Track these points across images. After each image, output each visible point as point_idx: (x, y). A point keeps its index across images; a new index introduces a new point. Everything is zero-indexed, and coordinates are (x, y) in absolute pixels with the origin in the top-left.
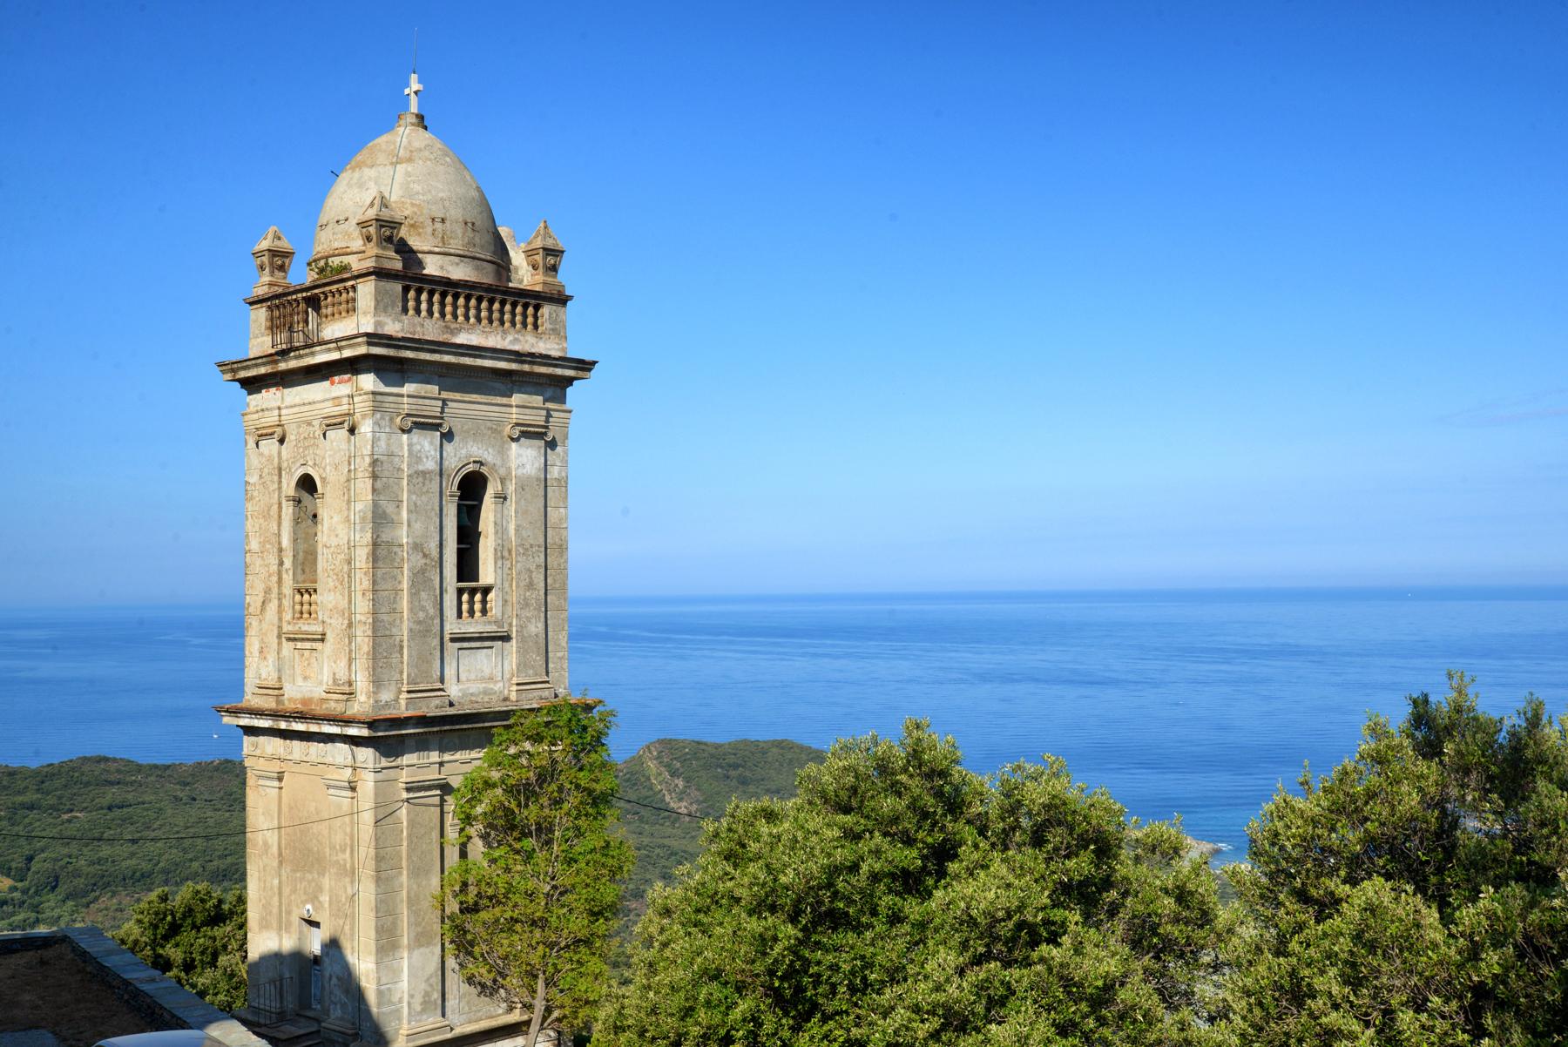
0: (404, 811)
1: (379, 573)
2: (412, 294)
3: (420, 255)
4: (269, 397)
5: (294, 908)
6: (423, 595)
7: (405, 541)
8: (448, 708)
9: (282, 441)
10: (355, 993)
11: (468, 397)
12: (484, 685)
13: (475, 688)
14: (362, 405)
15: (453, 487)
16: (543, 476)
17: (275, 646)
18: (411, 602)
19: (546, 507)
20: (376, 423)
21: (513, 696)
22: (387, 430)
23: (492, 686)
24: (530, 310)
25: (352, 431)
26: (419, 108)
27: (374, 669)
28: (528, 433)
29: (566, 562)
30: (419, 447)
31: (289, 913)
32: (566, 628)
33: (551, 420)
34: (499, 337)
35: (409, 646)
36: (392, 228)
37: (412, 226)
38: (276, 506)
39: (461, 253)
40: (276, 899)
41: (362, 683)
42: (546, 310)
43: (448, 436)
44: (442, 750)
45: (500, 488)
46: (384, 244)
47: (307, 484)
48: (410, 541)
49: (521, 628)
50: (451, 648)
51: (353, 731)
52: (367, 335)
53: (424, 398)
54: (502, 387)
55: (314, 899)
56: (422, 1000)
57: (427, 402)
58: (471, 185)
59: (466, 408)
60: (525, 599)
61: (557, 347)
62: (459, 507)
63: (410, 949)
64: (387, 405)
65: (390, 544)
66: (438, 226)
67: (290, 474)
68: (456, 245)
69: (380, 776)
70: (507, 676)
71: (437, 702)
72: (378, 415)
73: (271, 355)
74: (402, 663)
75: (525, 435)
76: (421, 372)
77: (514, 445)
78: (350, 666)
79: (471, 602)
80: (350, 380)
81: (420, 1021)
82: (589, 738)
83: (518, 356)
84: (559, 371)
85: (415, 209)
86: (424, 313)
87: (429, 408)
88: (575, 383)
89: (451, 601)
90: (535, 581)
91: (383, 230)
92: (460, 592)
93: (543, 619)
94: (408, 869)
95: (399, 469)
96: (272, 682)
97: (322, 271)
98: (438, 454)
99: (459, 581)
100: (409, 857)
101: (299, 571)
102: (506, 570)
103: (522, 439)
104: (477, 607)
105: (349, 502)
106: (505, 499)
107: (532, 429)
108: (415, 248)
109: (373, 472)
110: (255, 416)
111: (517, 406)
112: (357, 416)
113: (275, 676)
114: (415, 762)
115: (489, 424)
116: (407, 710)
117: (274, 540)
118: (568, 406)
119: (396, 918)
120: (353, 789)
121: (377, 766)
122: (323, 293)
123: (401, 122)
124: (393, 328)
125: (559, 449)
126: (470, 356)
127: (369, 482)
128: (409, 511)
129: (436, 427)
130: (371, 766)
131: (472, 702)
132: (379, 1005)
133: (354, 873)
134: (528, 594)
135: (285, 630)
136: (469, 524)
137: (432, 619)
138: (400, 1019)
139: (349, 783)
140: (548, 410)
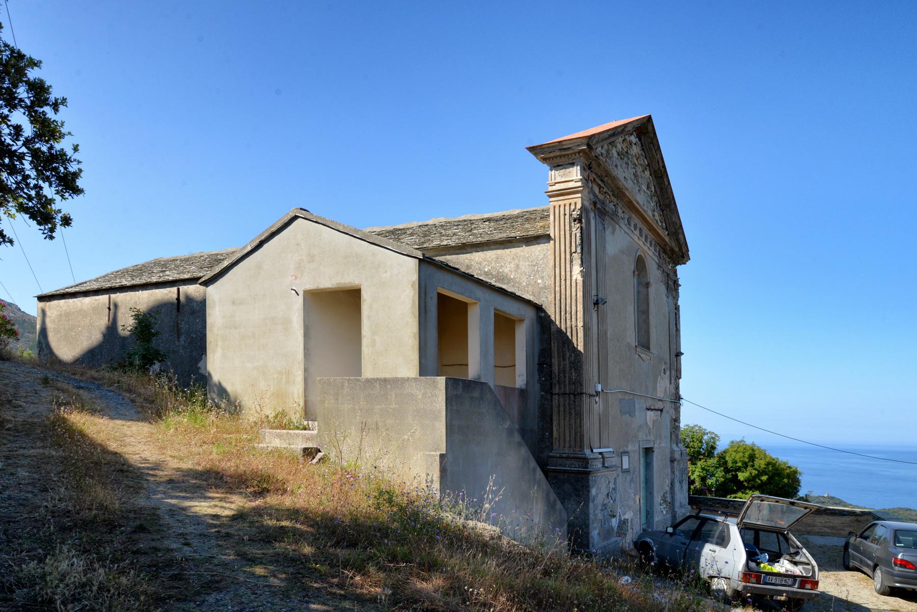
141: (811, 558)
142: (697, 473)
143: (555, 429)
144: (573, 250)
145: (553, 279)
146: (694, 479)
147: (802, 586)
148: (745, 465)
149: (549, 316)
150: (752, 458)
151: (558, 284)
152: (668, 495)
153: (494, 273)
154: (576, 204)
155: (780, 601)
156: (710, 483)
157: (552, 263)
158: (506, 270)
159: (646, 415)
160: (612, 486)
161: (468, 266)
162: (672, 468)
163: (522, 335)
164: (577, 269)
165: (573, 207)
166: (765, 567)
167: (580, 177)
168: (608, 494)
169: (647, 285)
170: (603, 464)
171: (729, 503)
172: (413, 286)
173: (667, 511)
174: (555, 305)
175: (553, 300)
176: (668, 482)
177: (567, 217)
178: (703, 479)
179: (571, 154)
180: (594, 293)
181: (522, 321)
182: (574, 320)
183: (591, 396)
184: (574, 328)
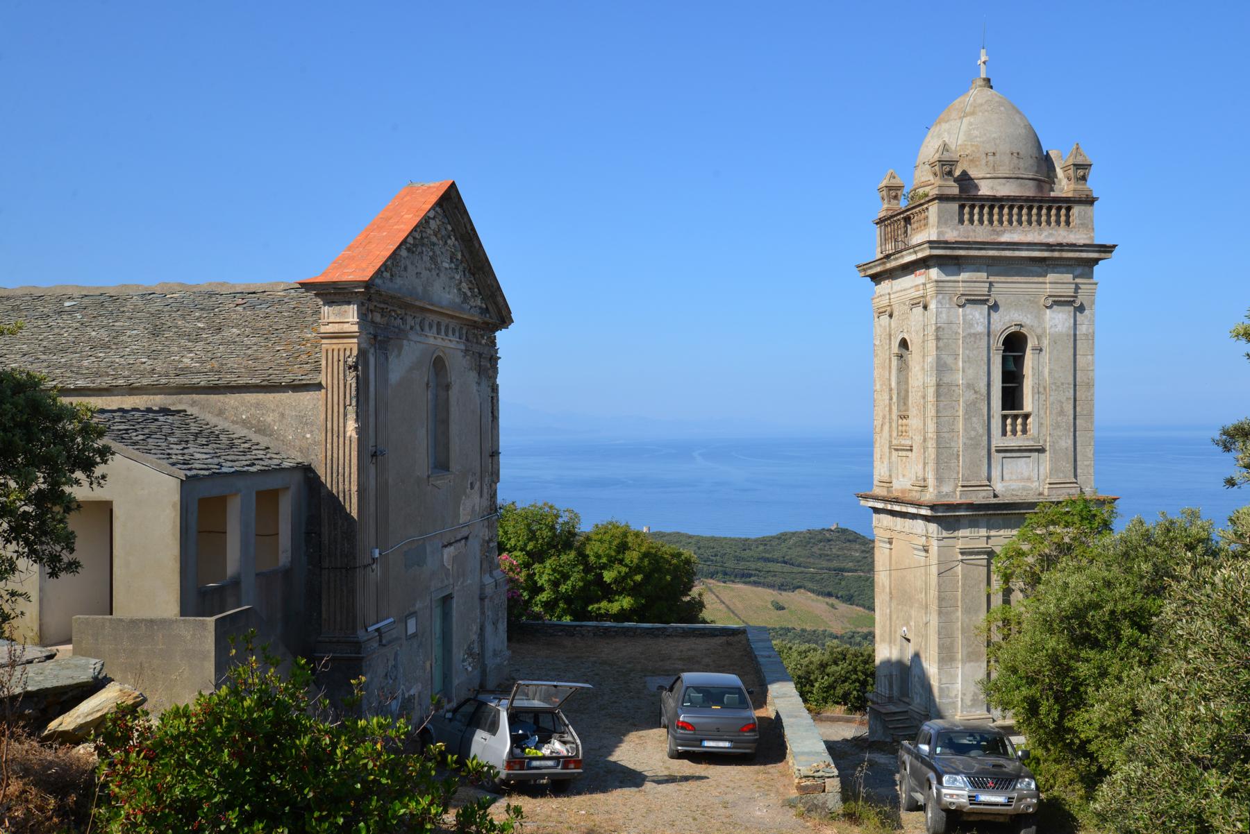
0: (959, 568)
1: (942, 404)
2: (967, 210)
3: (976, 181)
4: (886, 286)
5: (898, 629)
6: (974, 419)
7: (961, 382)
8: (992, 499)
9: (891, 316)
10: (928, 688)
11: (1010, 279)
12: (1023, 484)
13: (1015, 485)
14: (931, 288)
15: (998, 343)
16: (1072, 332)
17: (888, 454)
18: (965, 425)
19: (1075, 355)
20: (939, 302)
21: (1046, 492)
22: (947, 306)
23: (1029, 484)
24: (1063, 212)
25: (925, 307)
26: (987, 72)
27: (937, 470)
28: (1059, 302)
29: (1093, 395)
30: (971, 317)
31: (895, 632)
32: (1092, 444)
33: (1079, 291)
34: (1036, 234)
35: (963, 455)
36: (951, 165)
37: (972, 161)
38: (888, 360)
39: (1007, 176)
40: (888, 622)
41: (931, 481)
42: (1076, 210)
43: (995, 307)
44: (989, 528)
45: (1037, 343)
46: (946, 177)
47: (904, 344)
48: (965, 382)
49: (1053, 444)
50: (996, 457)
51: (924, 512)
52: (929, 242)
53: (975, 282)
54: (1039, 270)
55: (907, 624)
56: (971, 698)
57: (977, 284)
58: (1019, 125)
59: (1007, 287)
60: (1057, 423)
61: (1085, 236)
62: (1004, 358)
63: (963, 662)
64: (947, 289)
65: (949, 385)
66: (991, 158)
67: (896, 338)
68: (1004, 171)
69: (942, 543)
70: (1042, 477)
71: (984, 494)
72: (940, 296)
73: (881, 259)
74: (959, 466)
75: (1056, 303)
76: (973, 264)
77: (1048, 311)
78: (924, 468)
79: (1014, 425)
80: (925, 272)
81: (970, 712)
82: (1097, 524)
83: (1049, 247)
84: (1084, 255)
85: (974, 148)
86: (976, 222)
87: (979, 289)
88: (1100, 262)
89: (997, 424)
90: (1066, 409)
91: (944, 167)
92: (1005, 418)
93: (1072, 437)
94: (962, 608)
95: (957, 333)
96: (886, 479)
97: (912, 198)
98: (986, 321)
99: (1003, 409)
100: (963, 599)
101: (902, 404)
102: (1041, 402)
103: (1055, 307)
104: (1019, 428)
105: (924, 357)
106: (1041, 350)
107: (1063, 299)
108: (972, 176)
109: (937, 336)
110: (877, 300)
111: (1050, 283)
112: (928, 298)
113: (888, 474)
114: (968, 534)
115: (1027, 297)
116: (960, 498)
117: (887, 383)
118: (1095, 280)
119: (954, 641)
120: (927, 551)
121: (940, 536)
122: (912, 214)
123: (974, 86)
124: (951, 235)
125: (1087, 312)
126: (1009, 249)
127: (934, 342)
128: (964, 362)
129: (984, 302)
130: (935, 535)
131: (1013, 495)
132: (940, 697)
133: (927, 608)
134: (1059, 419)
135: (893, 443)
136: (1015, 369)
137: (981, 436)
138: (956, 708)
139: (923, 546)
140: (1077, 284)
141: (576, 737)
142: (545, 577)
143: (324, 609)
144: (348, 403)
145: (324, 435)
146: (543, 584)
147: (565, 767)
148: (612, 561)
149: (319, 477)
150: (623, 547)
151: (329, 441)
152: (476, 645)
153: (254, 422)
154: (351, 349)
155: (543, 784)
156: (564, 591)
157: (323, 416)
158: (269, 419)
159: (442, 555)
160: (392, 663)
161: (220, 410)
162: (482, 608)
163: (286, 507)
164: (351, 425)
165: (348, 353)
166: (531, 752)
167: (356, 320)
168: (386, 675)
169: (448, 387)
170: (380, 641)
171: (575, 629)
172: (174, 506)
173: (474, 668)
174: (326, 464)
175: (324, 459)
176: (475, 628)
177: (341, 363)
178: (556, 584)
179: (347, 293)
180: (372, 442)
181: (287, 488)
182: (347, 483)
183: (365, 567)
184: (347, 493)
